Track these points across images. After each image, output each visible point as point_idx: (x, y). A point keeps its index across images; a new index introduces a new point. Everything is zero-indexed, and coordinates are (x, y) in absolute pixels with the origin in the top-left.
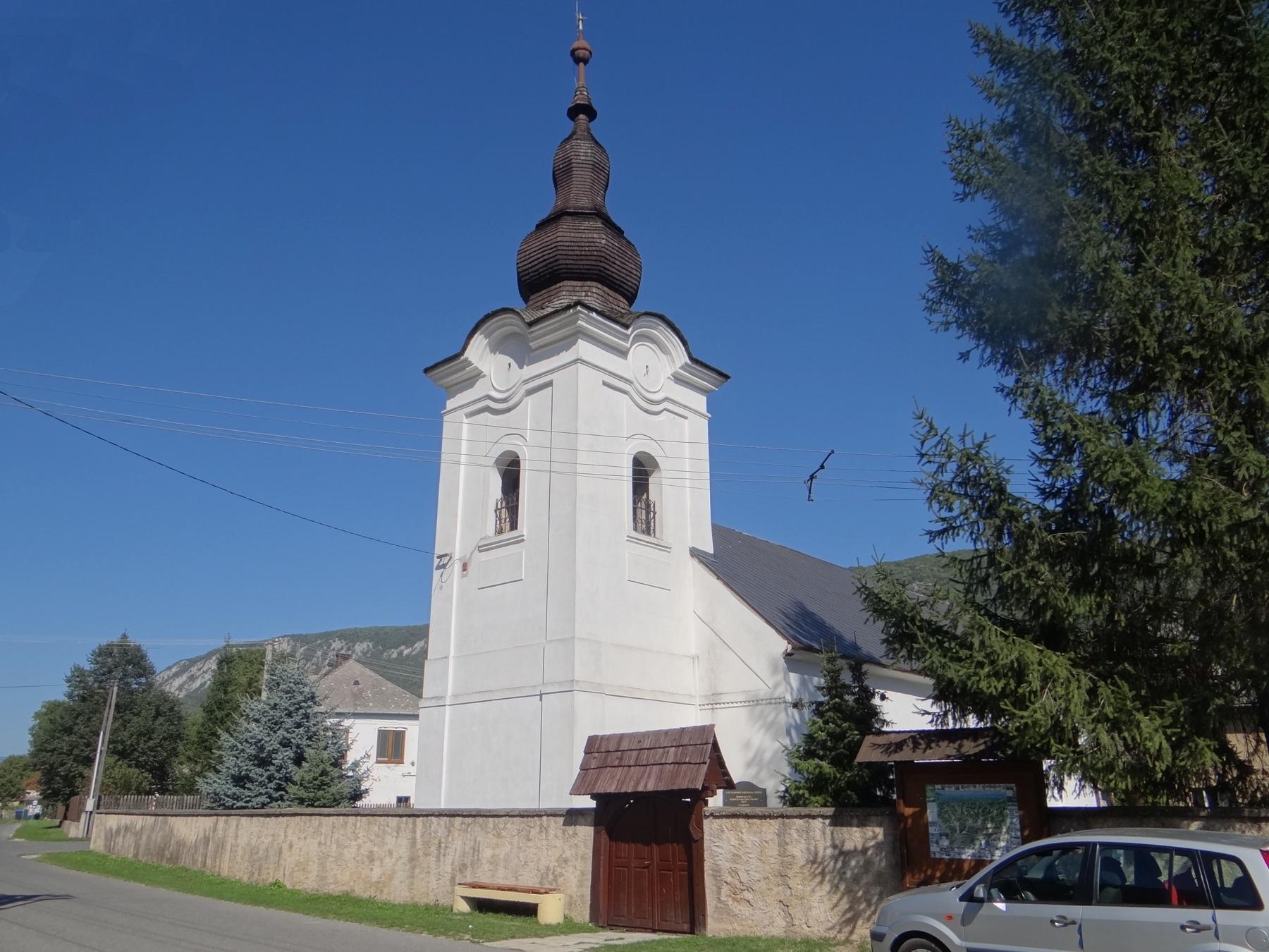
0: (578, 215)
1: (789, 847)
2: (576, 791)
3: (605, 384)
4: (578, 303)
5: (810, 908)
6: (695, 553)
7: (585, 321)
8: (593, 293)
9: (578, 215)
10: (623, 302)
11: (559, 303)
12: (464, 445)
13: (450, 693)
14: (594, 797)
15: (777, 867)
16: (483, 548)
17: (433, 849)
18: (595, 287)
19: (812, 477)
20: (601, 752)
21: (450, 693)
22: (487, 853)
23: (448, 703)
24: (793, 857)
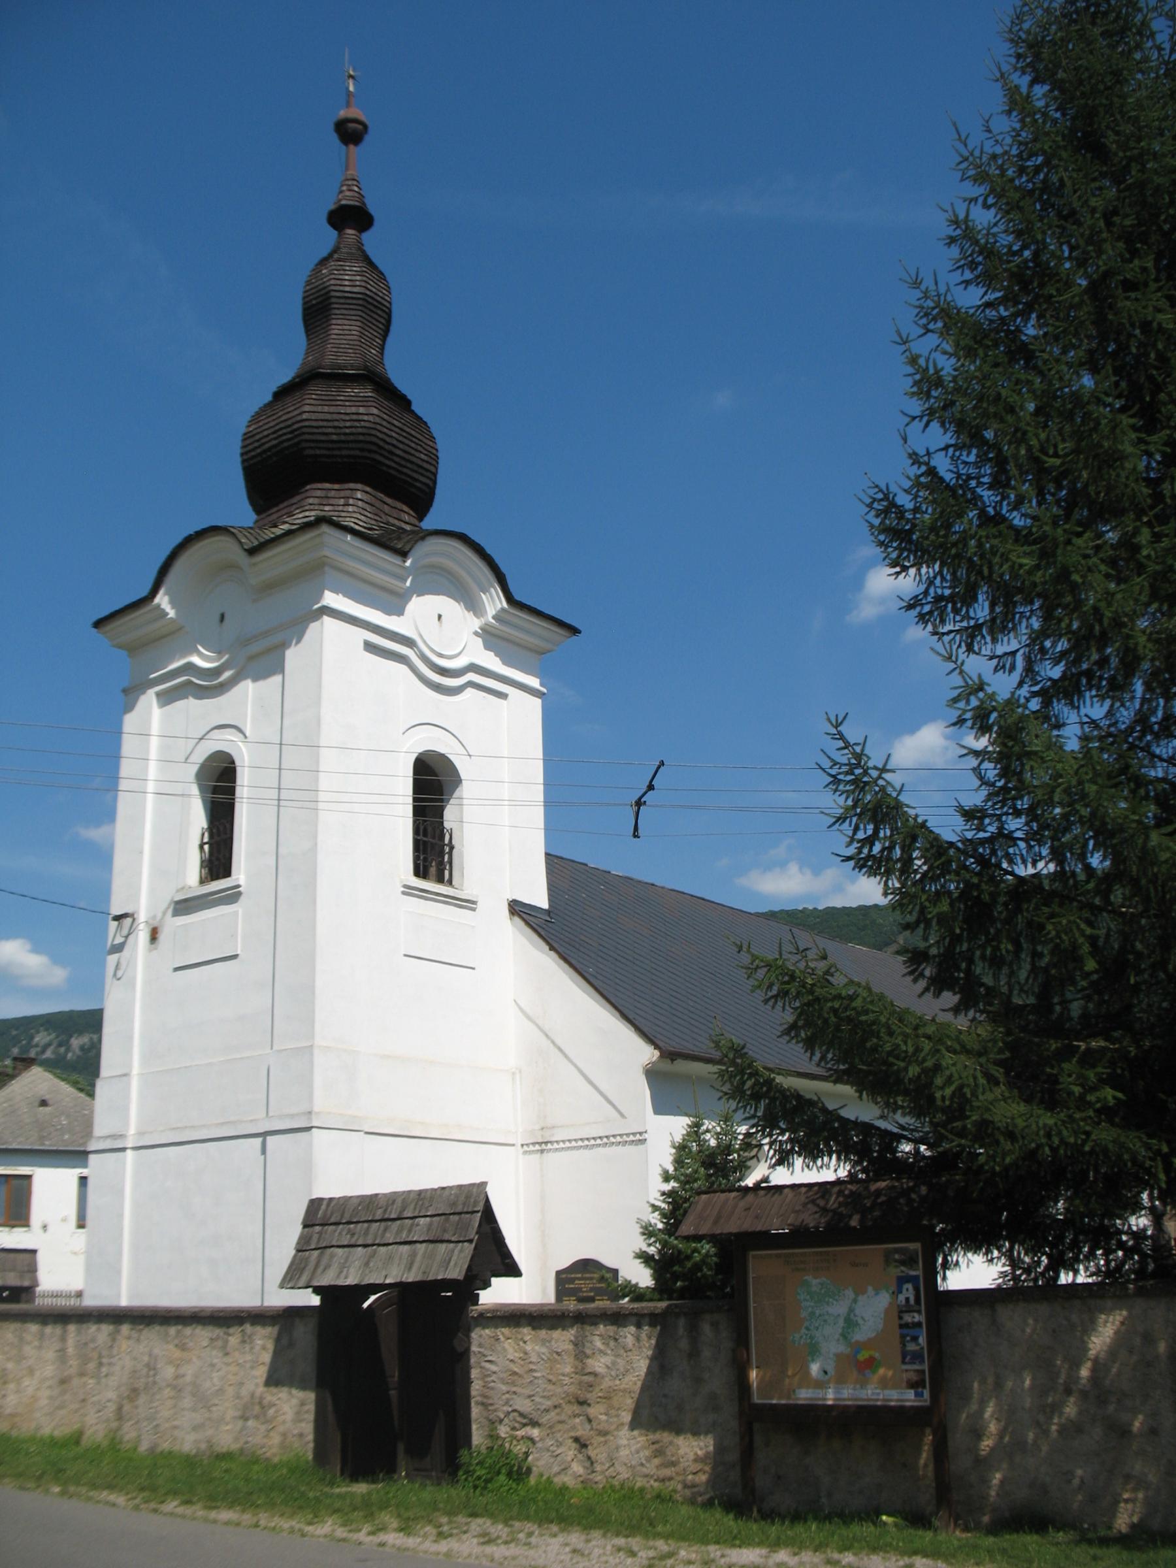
0: (339, 378)
1: (589, 1361)
2: (290, 1279)
3: (370, 647)
4: (319, 521)
5: (617, 1448)
6: (518, 909)
7: (334, 544)
8: (356, 503)
9: (339, 378)
10: (408, 515)
11: (300, 518)
12: (154, 742)
13: (132, 1131)
14: (317, 1290)
15: (572, 1389)
16: (184, 906)
17: (91, 1366)
18: (360, 493)
19: (639, 803)
20: (325, 1220)
21: (132, 1131)
22: (169, 1372)
23: (130, 1144)
24: (595, 1374)
